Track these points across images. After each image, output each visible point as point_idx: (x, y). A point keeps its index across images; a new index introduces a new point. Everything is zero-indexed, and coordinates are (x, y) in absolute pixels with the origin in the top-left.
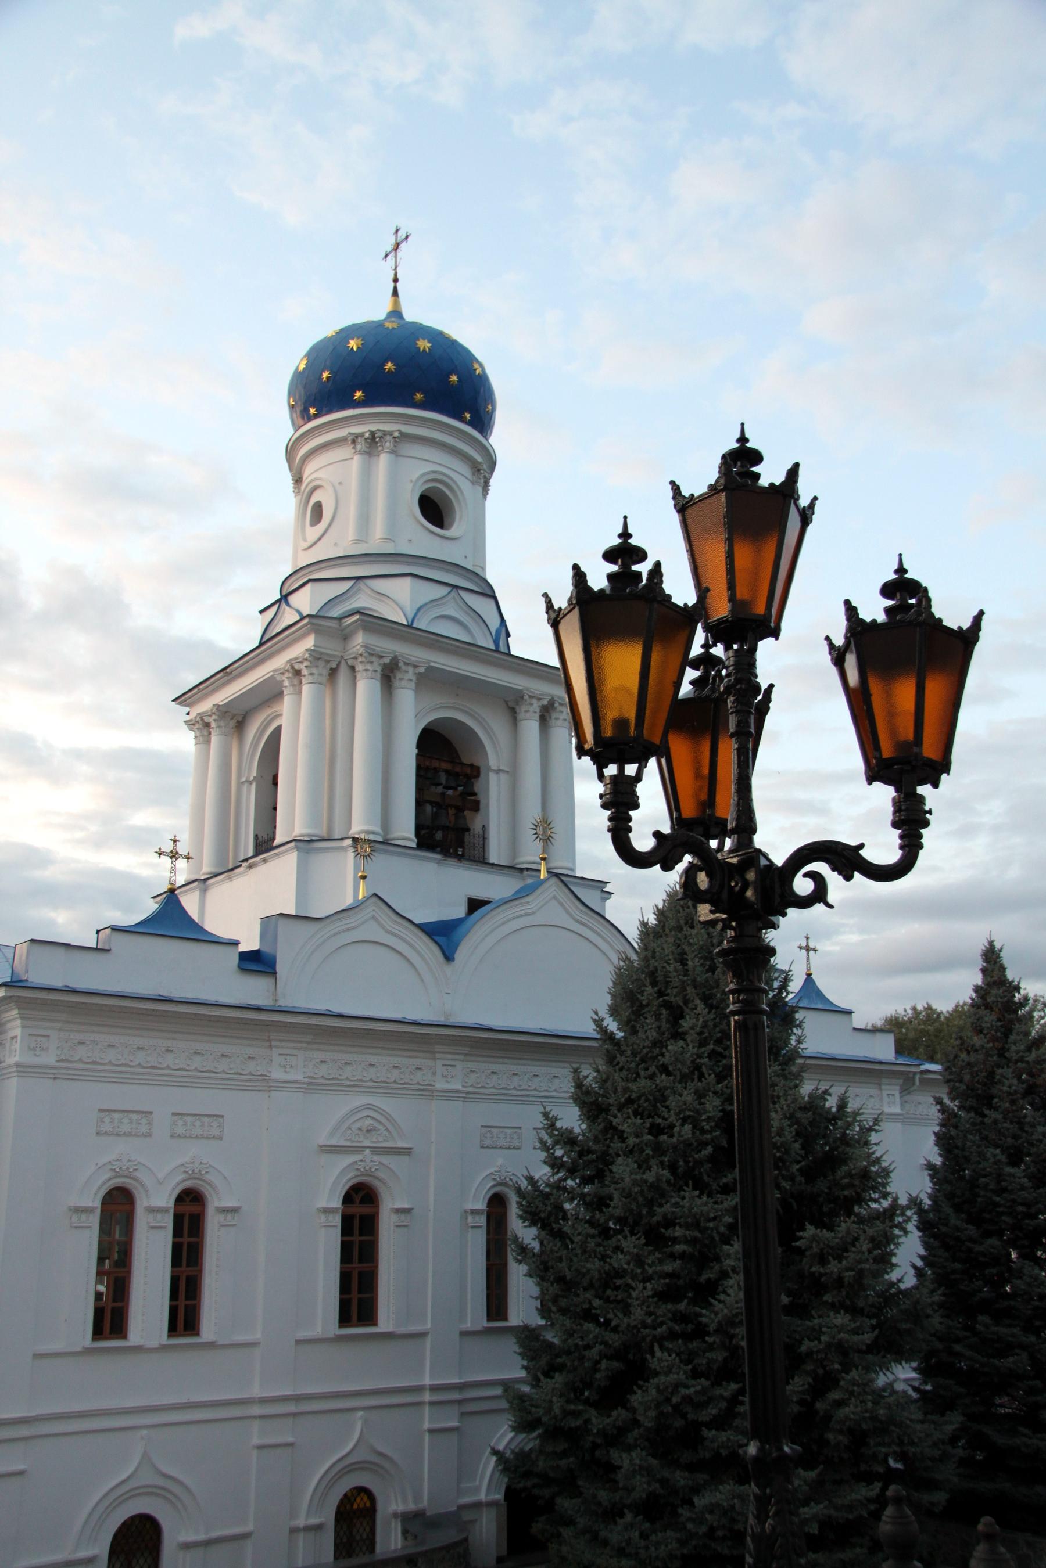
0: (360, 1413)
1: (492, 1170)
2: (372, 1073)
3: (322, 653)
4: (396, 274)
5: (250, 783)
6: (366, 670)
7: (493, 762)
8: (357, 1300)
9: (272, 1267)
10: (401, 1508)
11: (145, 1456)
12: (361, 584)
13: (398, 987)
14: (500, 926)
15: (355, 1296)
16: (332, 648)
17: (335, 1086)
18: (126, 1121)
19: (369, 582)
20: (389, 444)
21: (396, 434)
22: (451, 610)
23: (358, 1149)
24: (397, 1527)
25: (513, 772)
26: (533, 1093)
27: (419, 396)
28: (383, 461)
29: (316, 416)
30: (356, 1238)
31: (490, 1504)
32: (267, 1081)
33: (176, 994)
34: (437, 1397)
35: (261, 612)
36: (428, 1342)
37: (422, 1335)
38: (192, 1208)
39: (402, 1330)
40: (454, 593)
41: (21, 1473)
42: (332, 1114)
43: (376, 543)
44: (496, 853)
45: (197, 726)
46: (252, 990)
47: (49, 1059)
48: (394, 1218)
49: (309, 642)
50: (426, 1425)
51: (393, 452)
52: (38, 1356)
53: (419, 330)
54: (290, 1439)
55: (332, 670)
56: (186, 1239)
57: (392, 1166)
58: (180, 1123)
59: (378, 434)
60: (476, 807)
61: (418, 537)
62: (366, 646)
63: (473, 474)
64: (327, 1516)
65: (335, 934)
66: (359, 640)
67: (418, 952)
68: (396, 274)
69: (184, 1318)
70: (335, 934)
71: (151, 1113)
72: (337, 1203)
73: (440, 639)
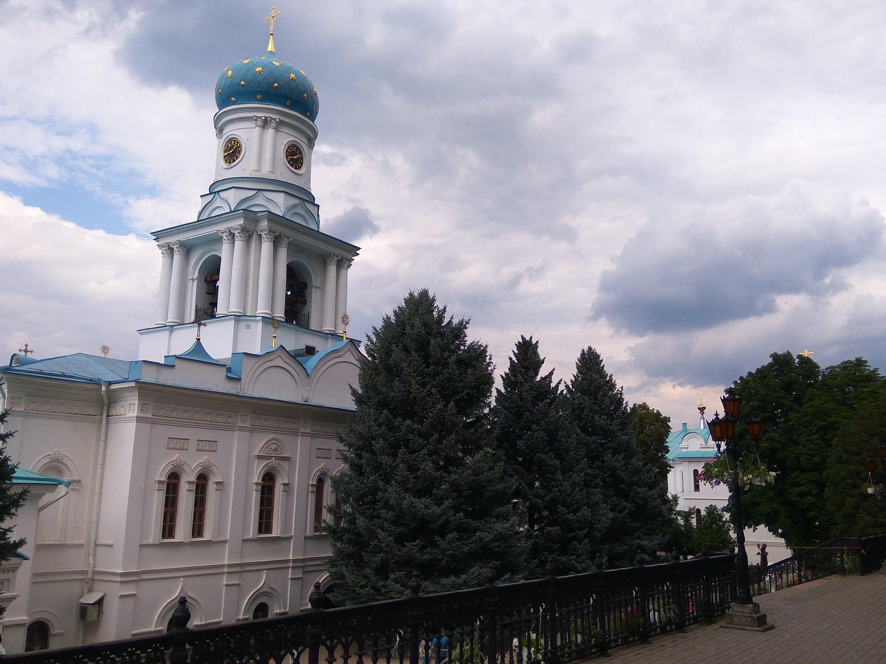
5: (194, 280)
7: (314, 283)
8: (265, 524)
12: (260, 193)
13: (282, 388)
15: (264, 521)
16: (250, 227)
17: (267, 430)
19: (264, 193)
25: (323, 288)
28: (270, 132)
29: (234, 103)
30: (266, 496)
34: (295, 565)
36: (227, 545)
39: (283, 536)
42: (261, 441)
43: (266, 171)
44: (313, 326)
47: (148, 415)
48: (215, 486)
50: (225, 583)
51: (276, 129)
60: (304, 303)
61: (284, 173)
69: (198, 529)
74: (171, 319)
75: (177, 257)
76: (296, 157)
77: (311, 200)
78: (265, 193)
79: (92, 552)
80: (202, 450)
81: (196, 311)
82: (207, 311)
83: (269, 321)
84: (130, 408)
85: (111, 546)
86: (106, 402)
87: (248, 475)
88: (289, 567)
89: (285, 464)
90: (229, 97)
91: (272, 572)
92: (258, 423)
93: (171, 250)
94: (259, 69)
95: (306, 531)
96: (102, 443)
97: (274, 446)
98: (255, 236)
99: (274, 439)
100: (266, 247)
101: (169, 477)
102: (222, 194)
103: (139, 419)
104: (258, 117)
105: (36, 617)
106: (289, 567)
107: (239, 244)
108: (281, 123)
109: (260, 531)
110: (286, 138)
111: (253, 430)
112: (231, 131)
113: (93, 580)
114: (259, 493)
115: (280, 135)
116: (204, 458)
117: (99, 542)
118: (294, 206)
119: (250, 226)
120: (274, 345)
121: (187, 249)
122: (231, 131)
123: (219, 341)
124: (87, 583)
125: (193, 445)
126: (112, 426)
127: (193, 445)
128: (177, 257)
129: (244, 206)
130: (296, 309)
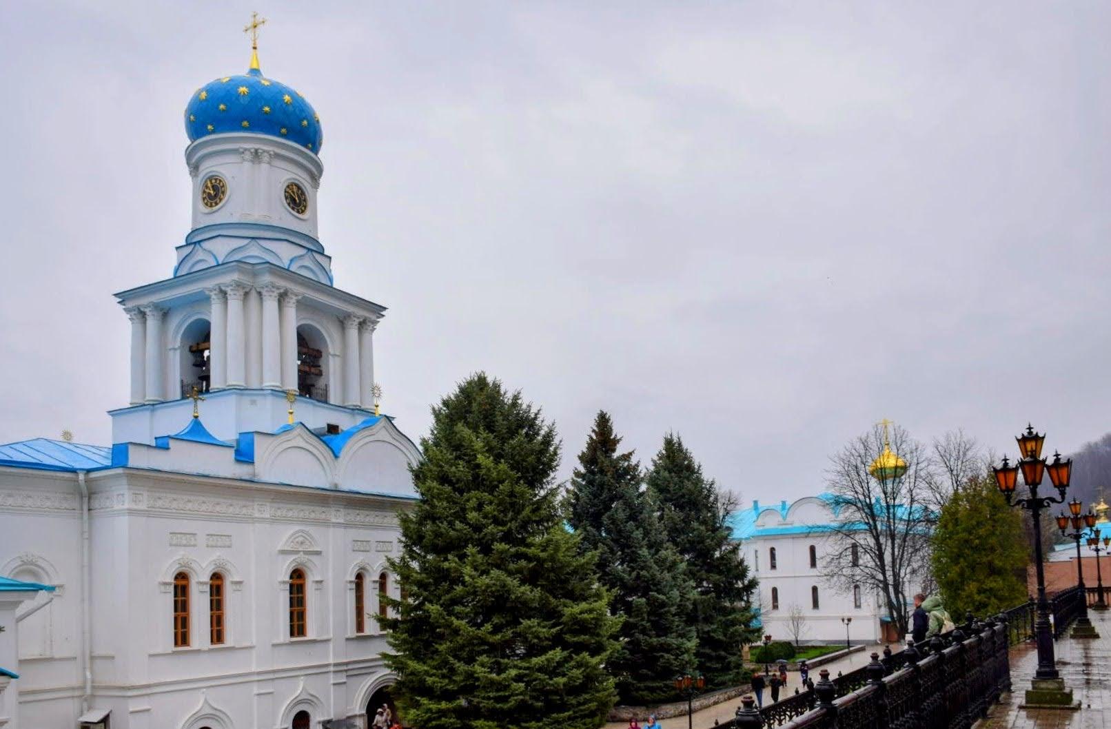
2: (313, 515)
7: (331, 351)
8: (297, 625)
9: (257, 611)
10: (322, 719)
11: (206, 702)
15: (296, 623)
16: (245, 279)
17: (291, 521)
23: (297, 552)
25: (344, 357)
27: (245, 123)
29: (213, 132)
36: (331, 645)
37: (328, 641)
38: (218, 582)
40: (253, 242)
41: (148, 710)
42: (285, 535)
43: (256, 216)
44: (334, 398)
46: (243, 471)
47: (142, 506)
48: (315, 586)
52: (151, 656)
56: (215, 598)
60: (320, 374)
61: (284, 217)
66: (267, 278)
69: (217, 635)
72: (287, 578)
74: (151, 396)
76: (297, 200)
79: (88, 665)
80: (176, 545)
81: (182, 387)
85: (113, 658)
90: (204, 125)
97: (301, 539)
98: (253, 295)
99: (302, 531)
100: (271, 305)
101: (176, 578)
102: (206, 245)
107: (234, 304)
112: (208, 167)
113: (93, 696)
114: (288, 593)
116: (216, 554)
117: (97, 652)
122: (208, 167)
123: (221, 417)
124: (86, 700)
128: (152, 323)
129: (237, 257)
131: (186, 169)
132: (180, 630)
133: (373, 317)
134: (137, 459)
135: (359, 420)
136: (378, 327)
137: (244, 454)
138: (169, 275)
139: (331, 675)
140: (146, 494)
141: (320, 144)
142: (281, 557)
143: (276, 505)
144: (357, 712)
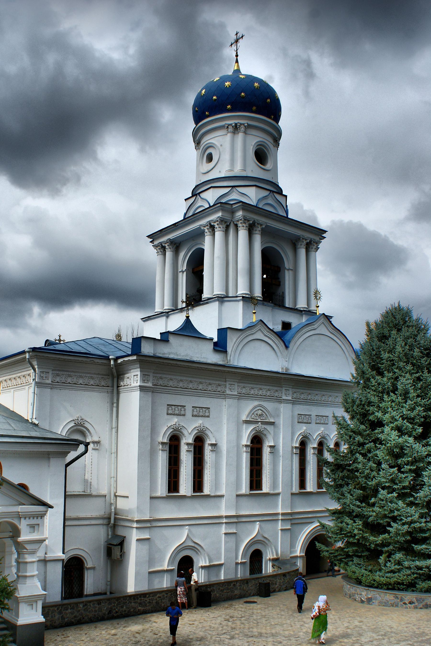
0: (258, 523)
1: (320, 432)
3: (224, 219)
4: (237, 53)
6: (243, 226)
7: (287, 266)
8: (256, 482)
12: (234, 189)
14: (304, 334)
15: (173, 480)
16: (227, 216)
18: (177, 409)
19: (238, 188)
20: (243, 129)
21: (246, 125)
22: (270, 201)
23: (257, 422)
24: (270, 564)
25: (295, 271)
26: (315, 401)
28: (240, 136)
31: (300, 557)
32: (225, 395)
33: (195, 359)
35: (186, 200)
36: (224, 500)
39: (272, 492)
40: (271, 194)
42: (247, 408)
43: (238, 170)
44: (288, 303)
45: (158, 248)
46: (213, 358)
47: (150, 384)
48: (210, 448)
49: (220, 214)
51: (245, 133)
53: (251, 79)
54: (235, 531)
55: (228, 225)
56: (197, 456)
57: (268, 429)
58: (170, 408)
59: (239, 124)
61: (254, 170)
62: (244, 216)
63: (274, 142)
64: (247, 560)
65: (247, 336)
67: (276, 344)
68: (237, 53)
69: (198, 485)
70: (247, 336)
71: (185, 406)
73: (271, 214)
74: (167, 306)
75: (169, 254)
76: (261, 156)
77: (280, 192)
78: (239, 189)
82: (195, 299)
83: (248, 299)
84: (134, 378)
85: (128, 497)
86: (115, 374)
87: (239, 437)
88: (278, 520)
89: (270, 428)
91: (192, 527)
92: (244, 391)
93: (164, 248)
94: (227, 84)
95: (292, 489)
96: (115, 409)
97: (260, 412)
98: (232, 225)
99: (260, 406)
100: (243, 234)
102: (202, 195)
103: (142, 389)
104: (229, 125)
105: (71, 554)
106: (278, 520)
107: (219, 235)
108: (249, 126)
109: (252, 488)
110: (254, 140)
111: (240, 397)
114: (249, 455)
115: (249, 138)
118: (265, 198)
119: (228, 216)
120: (254, 319)
121: (176, 246)
123: (207, 320)
125: (189, 412)
126: (122, 396)
127: (189, 412)
128: (169, 254)
130: (272, 292)
131: (193, 145)
132: (197, 480)
133: (317, 238)
134: (147, 349)
135: (304, 319)
136: (320, 246)
137: (220, 346)
138: (183, 219)
139: (224, 525)
140: (236, 384)
141: (280, 116)
142: (244, 426)
143: (242, 385)
144: (298, 554)
